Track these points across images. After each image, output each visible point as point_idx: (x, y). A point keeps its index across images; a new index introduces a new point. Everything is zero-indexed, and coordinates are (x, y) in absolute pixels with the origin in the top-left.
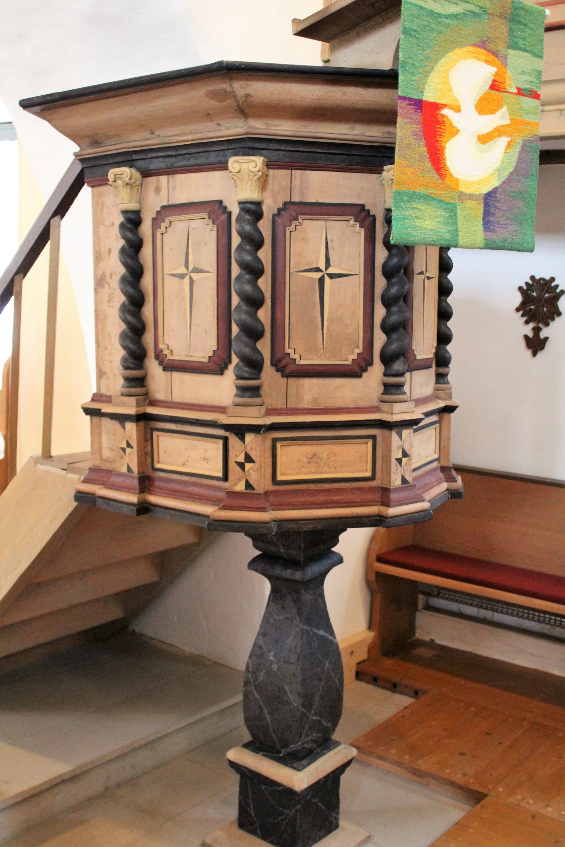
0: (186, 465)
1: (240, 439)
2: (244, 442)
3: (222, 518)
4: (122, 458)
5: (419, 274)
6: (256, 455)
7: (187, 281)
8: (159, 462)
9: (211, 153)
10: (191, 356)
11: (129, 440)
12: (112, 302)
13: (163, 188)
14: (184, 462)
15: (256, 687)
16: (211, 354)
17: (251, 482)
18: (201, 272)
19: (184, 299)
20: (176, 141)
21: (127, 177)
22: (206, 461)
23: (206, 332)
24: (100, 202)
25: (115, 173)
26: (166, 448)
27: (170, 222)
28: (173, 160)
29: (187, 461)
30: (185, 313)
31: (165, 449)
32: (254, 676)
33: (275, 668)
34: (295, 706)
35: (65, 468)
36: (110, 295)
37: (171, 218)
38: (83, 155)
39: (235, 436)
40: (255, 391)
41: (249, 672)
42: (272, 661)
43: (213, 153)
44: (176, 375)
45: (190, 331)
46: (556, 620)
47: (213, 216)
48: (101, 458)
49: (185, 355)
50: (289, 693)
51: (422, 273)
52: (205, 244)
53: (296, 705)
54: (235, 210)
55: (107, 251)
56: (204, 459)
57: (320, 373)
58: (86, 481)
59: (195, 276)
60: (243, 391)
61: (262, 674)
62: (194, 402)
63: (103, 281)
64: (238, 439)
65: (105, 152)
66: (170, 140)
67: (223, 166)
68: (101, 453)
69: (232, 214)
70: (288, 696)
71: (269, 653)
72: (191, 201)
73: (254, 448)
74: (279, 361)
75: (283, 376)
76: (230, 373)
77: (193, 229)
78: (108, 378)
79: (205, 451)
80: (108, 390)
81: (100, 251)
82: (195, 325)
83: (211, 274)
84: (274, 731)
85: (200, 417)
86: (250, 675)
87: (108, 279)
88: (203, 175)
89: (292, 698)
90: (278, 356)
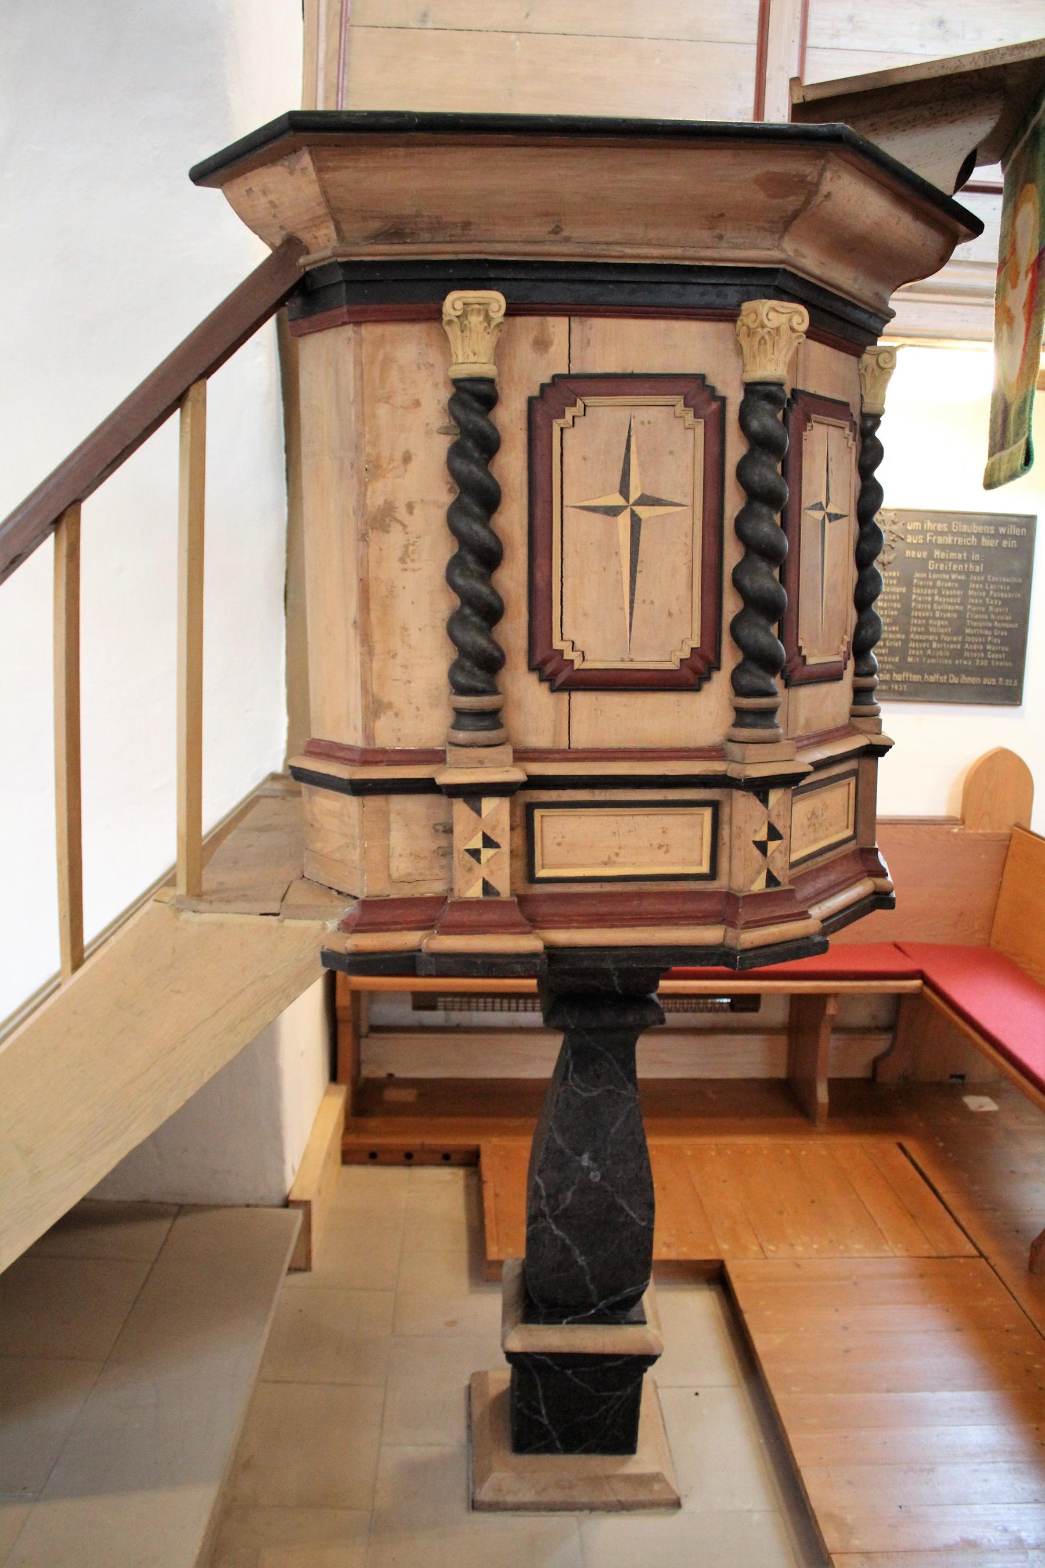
0: (614, 862)
1: (761, 801)
2: (767, 806)
3: (757, 943)
4: (470, 870)
5: (837, 517)
6: (785, 826)
7: (624, 521)
8: (543, 867)
9: (689, 288)
10: (632, 660)
11: (489, 833)
12: (413, 561)
13: (556, 341)
14: (609, 858)
15: (556, 1219)
16: (686, 654)
17: (775, 874)
18: (660, 505)
19: (617, 553)
20: (617, 254)
21: (499, 310)
22: (664, 849)
23: (670, 614)
24: (380, 356)
25: (465, 300)
26: (563, 837)
27: (585, 406)
28: (594, 290)
29: (617, 854)
30: (620, 582)
31: (559, 840)
32: (552, 1201)
33: (595, 1177)
34: (644, 1226)
35: (275, 911)
36: (406, 547)
37: (589, 400)
38: (351, 255)
39: (755, 797)
40: (491, 718)
41: (541, 1197)
42: (588, 1168)
43: (695, 288)
44: (582, 700)
45: (631, 614)
46: (445, 1002)
47: (693, 402)
48: (389, 876)
49: (619, 659)
50: (627, 1208)
51: (834, 517)
52: (671, 453)
53: (643, 1224)
54: (735, 398)
55: (398, 456)
56: (660, 847)
57: (818, 678)
58: (352, 926)
59: (643, 512)
60: (742, 717)
61: (569, 1194)
62: (630, 745)
63: (387, 520)
64: (758, 802)
65: (426, 254)
66: (603, 250)
67: (730, 315)
68: (388, 867)
69: (727, 401)
70: (627, 1214)
71: (580, 1155)
72: (629, 371)
73: (782, 813)
74: (545, 662)
75: (553, 690)
76: (719, 685)
77: (642, 423)
78: (397, 715)
79: (664, 832)
80: (399, 739)
81: (378, 457)
82: (644, 601)
83: (684, 508)
84: (593, 1278)
85: (672, 771)
86: (543, 1202)
87: (402, 513)
88: (661, 324)
89: (634, 1216)
90: (538, 657)
